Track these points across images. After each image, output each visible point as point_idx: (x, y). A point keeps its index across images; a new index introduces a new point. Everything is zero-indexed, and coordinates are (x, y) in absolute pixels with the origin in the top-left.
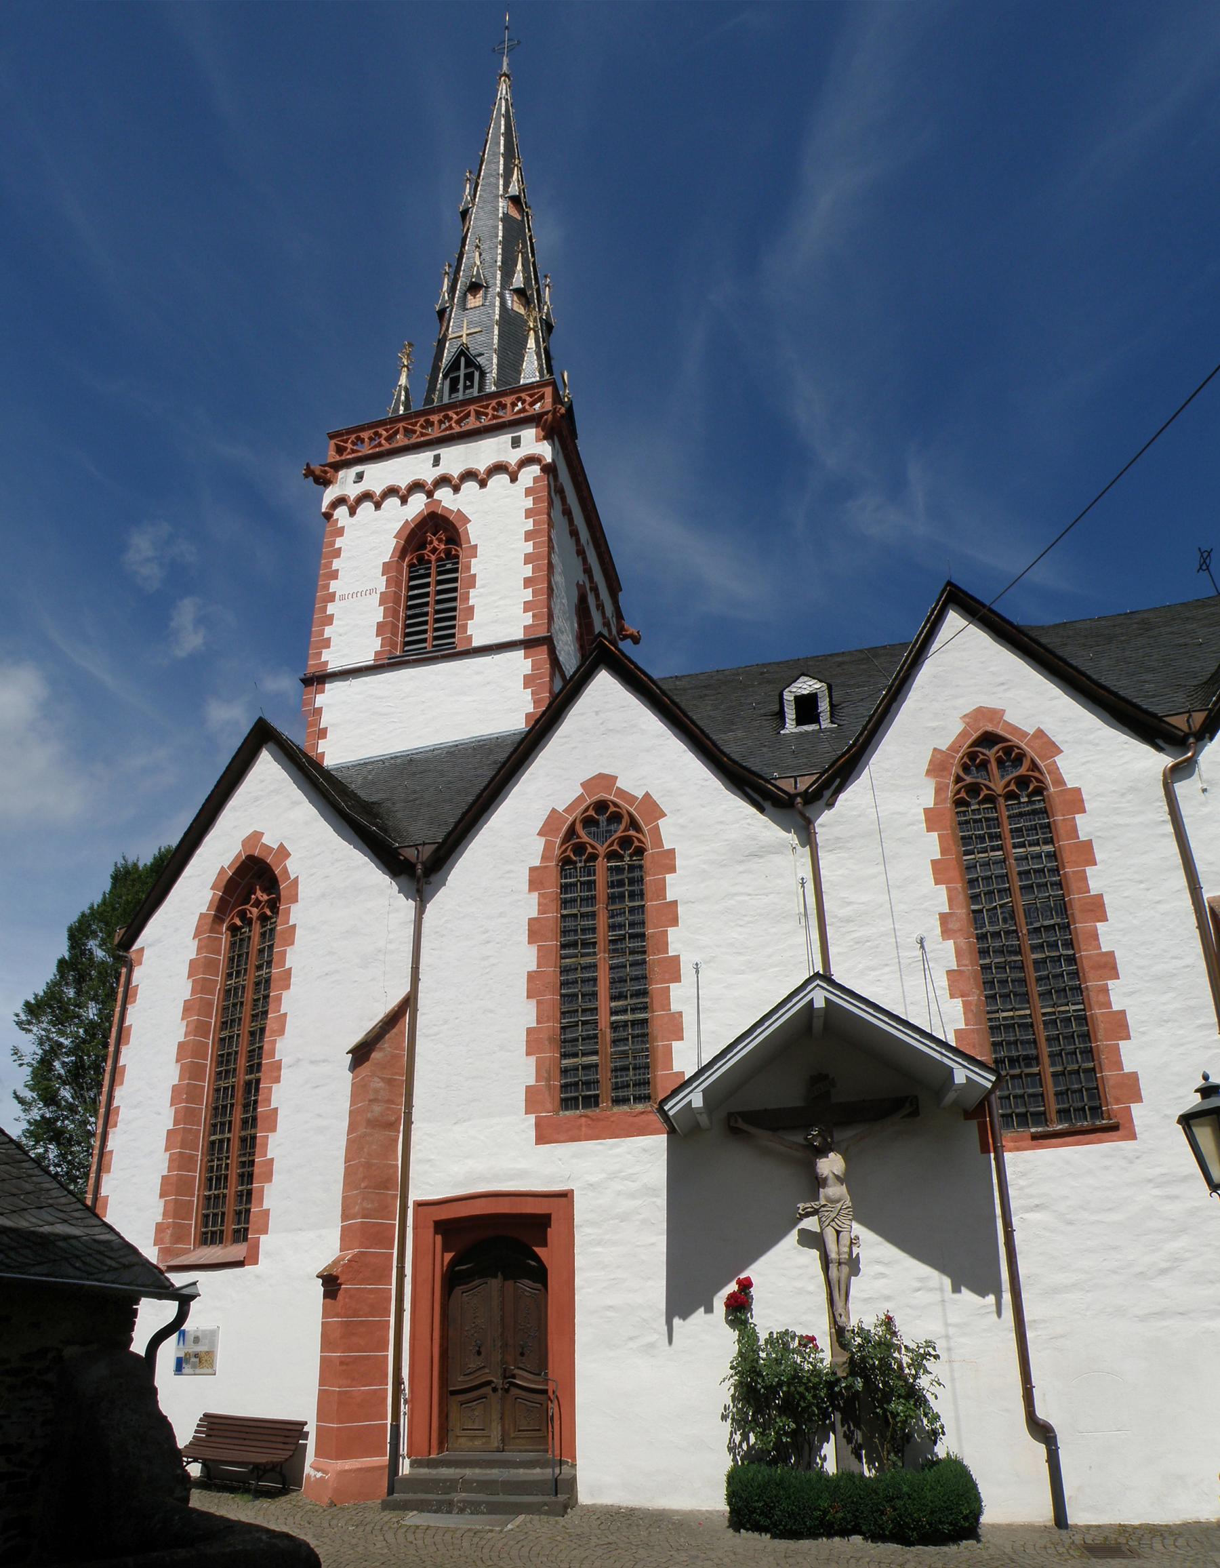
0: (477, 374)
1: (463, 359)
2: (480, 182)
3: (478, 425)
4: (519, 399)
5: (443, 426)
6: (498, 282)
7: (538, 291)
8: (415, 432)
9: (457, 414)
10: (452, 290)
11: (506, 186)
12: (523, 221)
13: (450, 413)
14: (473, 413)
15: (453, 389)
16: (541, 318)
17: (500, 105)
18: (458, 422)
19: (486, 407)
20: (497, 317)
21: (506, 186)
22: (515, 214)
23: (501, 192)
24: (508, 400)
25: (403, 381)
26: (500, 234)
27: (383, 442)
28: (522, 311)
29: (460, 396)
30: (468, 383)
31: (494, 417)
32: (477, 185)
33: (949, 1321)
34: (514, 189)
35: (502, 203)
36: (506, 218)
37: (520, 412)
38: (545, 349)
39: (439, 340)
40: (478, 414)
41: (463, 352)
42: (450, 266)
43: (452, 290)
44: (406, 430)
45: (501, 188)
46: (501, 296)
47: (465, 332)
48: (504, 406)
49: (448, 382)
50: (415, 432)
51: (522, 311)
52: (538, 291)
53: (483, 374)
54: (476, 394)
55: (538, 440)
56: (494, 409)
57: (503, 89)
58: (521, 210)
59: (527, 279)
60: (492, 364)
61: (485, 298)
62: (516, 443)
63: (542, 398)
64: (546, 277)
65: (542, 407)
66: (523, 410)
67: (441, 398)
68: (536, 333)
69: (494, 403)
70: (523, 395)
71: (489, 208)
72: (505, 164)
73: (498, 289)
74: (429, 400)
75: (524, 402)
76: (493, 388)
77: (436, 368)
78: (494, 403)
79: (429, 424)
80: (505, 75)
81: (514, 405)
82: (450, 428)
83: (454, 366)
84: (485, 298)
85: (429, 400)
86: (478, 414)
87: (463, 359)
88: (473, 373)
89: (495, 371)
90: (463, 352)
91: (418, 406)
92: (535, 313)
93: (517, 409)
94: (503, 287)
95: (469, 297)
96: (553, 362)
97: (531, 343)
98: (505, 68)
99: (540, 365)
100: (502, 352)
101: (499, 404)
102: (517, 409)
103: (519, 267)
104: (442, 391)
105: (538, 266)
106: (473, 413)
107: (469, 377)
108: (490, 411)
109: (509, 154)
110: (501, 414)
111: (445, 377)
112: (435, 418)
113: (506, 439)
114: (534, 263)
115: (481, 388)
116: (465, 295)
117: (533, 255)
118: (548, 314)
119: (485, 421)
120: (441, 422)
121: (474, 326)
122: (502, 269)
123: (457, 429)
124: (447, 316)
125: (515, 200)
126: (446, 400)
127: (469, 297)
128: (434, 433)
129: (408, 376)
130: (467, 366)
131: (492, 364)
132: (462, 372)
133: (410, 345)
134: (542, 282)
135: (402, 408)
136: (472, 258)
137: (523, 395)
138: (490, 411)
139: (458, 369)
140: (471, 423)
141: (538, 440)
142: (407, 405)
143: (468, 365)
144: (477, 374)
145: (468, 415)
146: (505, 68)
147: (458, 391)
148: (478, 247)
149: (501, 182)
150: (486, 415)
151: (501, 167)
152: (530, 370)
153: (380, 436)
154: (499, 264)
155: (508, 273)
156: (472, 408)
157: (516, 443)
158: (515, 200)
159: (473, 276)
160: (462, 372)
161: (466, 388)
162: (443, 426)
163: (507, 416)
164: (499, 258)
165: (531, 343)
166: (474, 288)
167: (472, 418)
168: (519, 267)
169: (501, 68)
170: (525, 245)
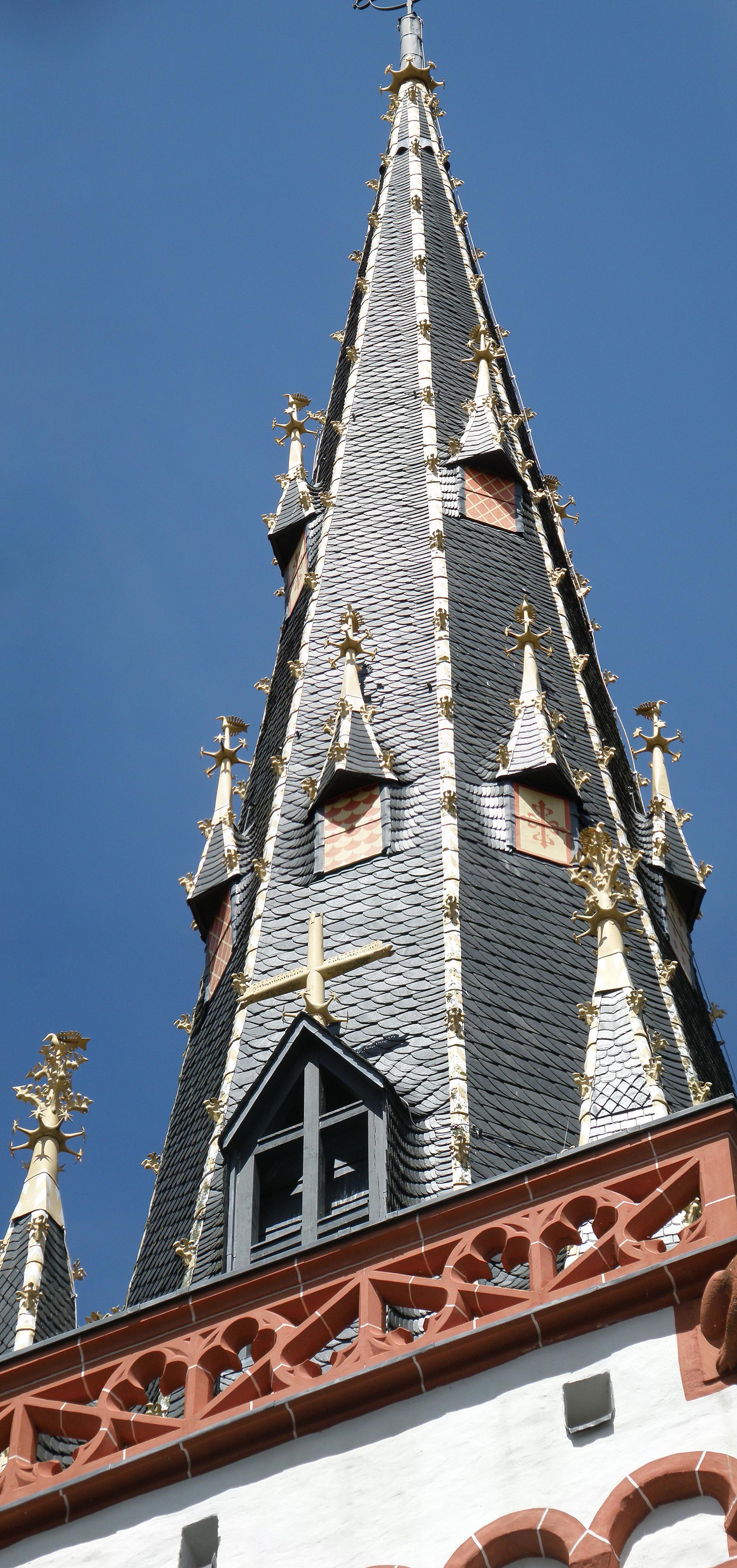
0: (378, 1129)
1: (311, 1074)
2: (345, 427)
3: (397, 1351)
4: (582, 1210)
5: (230, 1381)
6: (447, 762)
7: (620, 769)
8: (85, 1428)
9: (294, 1314)
10: (254, 811)
11: (450, 427)
12: (528, 533)
13: (264, 1316)
14: (369, 1301)
15: (275, 1199)
16: (644, 871)
17: (403, 172)
18: (301, 1352)
19: (434, 1263)
20: (452, 889)
21: (450, 427)
22: (489, 510)
23: (431, 451)
24: (531, 1223)
25: (36, 1196)
26: (441, 588)
27: (280, 1367)
28: (557, 850)
29: (307, 1228)
30: (342, 1169)
31: (473, 1306)
32: (331, 440)
33: (625, 1097)
34: (481, 435)
35: (440, 494)
36: (459, 534)
37: (591, 1266)
38: (678, 982)
39: (204, 1008)
40: (396, 1302)
41: (311, 1044)
42: (238, 728)
43: (254, 811)
44: (43, 1424)
45: (430, 436)
46: (463, 807)
47: (313, 964)
48: (516, 1253)
49: (245, 1179)
50: (85, 1428)
51: (557, 850)
52: (620, 769)
53: (406, 1123)
54: (379, 1212)
55: (696, 1386)
56: (470, 1269)
57: (409, 119)
58: (520, 502)
59: (566, 733)
60: (440, 1076)
61: (395, 824)
62: (589, 1415)
63: (688, 1191)
64: (646, 712)
65: (696, 1232)
66: (608, 1257)
67: (218, 1249)
68: (628, 929)
69: (465, 1242)
70: (599, 1192)
71: (387, 507)
72: (436, 359)
73: (450, 786)
74: (160, 1267)
75: (605, 1220)
76: (458, 1179)
77: (191, 1123)
78: (465, 1242)
79: (168, 1378)
80: (413, 75)
81: (559, 1238)
82: (266, 1381)
83: (277, 1101)
84: (395, 824)
85: (160, 1267)
86: (396, 1302)
87: (311, 1074)
88: (360, 1125)
89: (461, 1101)
90: (311, 1044)
91: (105, 1300)
92: (618, 853)
93: (574, 1255)
94: (467, 774)
95: (326, 827)
96: (722, 1029)
97: (612, 970)
98: (411, 51)
99: (664, 1054)
100: (485, 1021)
101: (491, 1243)
102: (574, 1255)
103: (530, 689)
104: (220, 1217)
105: (609, 677)
106: (369, 1301)
107: (346, 1142)
108: (450, 1282)
109: (451, 321)
110: (502, 1283)
111: (233, 1157)
112: (188, 1349)
113: (534, 1401)
114: (591, 672)
115: (400, 1186)
116: (309, 821)
117: (559, 560)
118: (670, 847)
119: (430, 1332)
120: (217, 1362)
121: (361, 937)
122: (454, 711)
123: (297, 1384)
124: (233, 909)
125: (491, 469)
126: (240, 1258)
127: (326, 827)
128: (187, 1417)
129: (60, 1175)
130: (329, 1103)
131: (440, 1076)
132: (311, 1128)
133: (71, 1043)
134: (631, 733)
135: (26, 1320)
136: (325, 683)
137: (599, 1192)
138: (450, 1282)
139: (294, 1114)
140: (367, 1348)
141: (696, 1386)
142: (52, 1304)
143: (334, 1094)
144: (378, 1129)
145: (347, 1313)
146: (411, 51)
147: (295, 1206)
148: (350, 647)
149: (429, 417)
150: (434, 1300)
151: (425, 369)
152: (621, 1077)
153: (262, 1342)
154: (444, 692)
155: (481, 713)
156: (364, 1277)
157: (589, 1415)
158: (491, 469)
159: (337, 753)
160: (311, 1128)
161: (331, 1189)
162: (230, 1381)
163: (538, 1291)
164: (444, 673)
165: (612, 970)
166: (345, 792)
167: (368, 1324)
168: (530, 689)
169: (396, 54)
170: (544, 614)
